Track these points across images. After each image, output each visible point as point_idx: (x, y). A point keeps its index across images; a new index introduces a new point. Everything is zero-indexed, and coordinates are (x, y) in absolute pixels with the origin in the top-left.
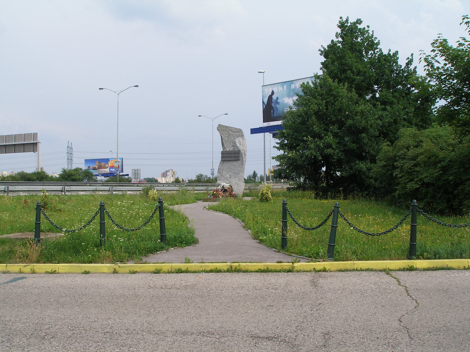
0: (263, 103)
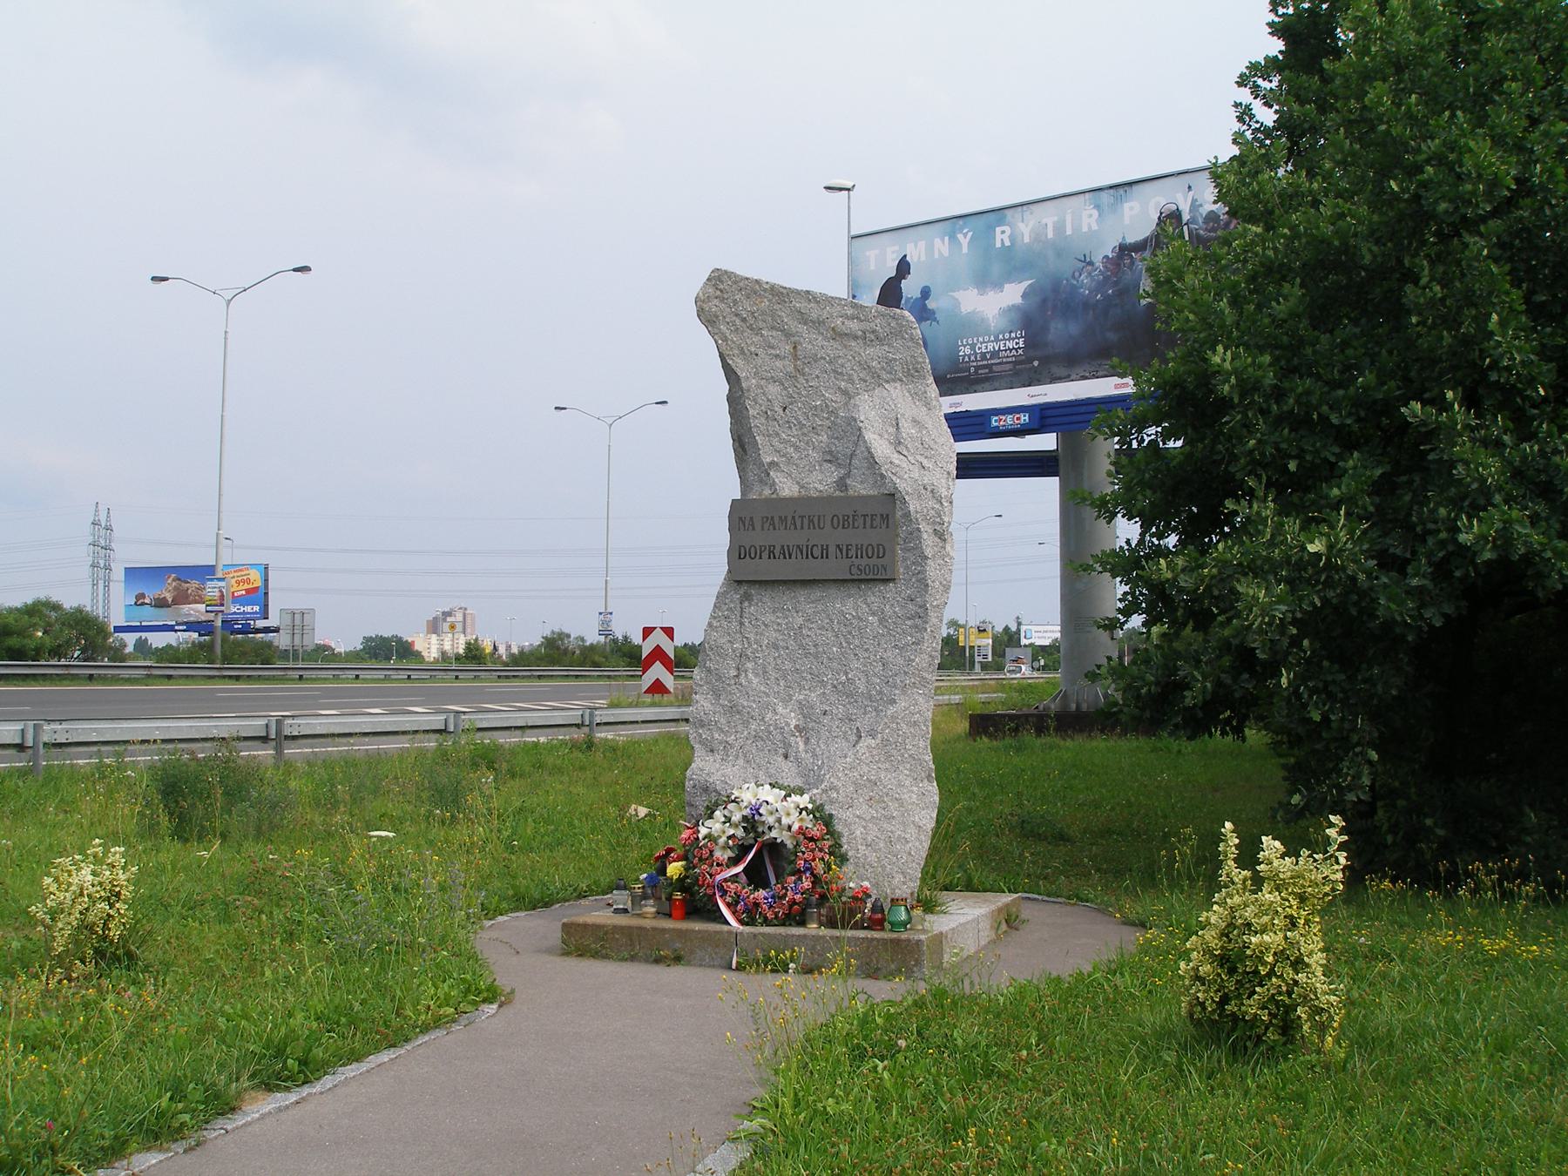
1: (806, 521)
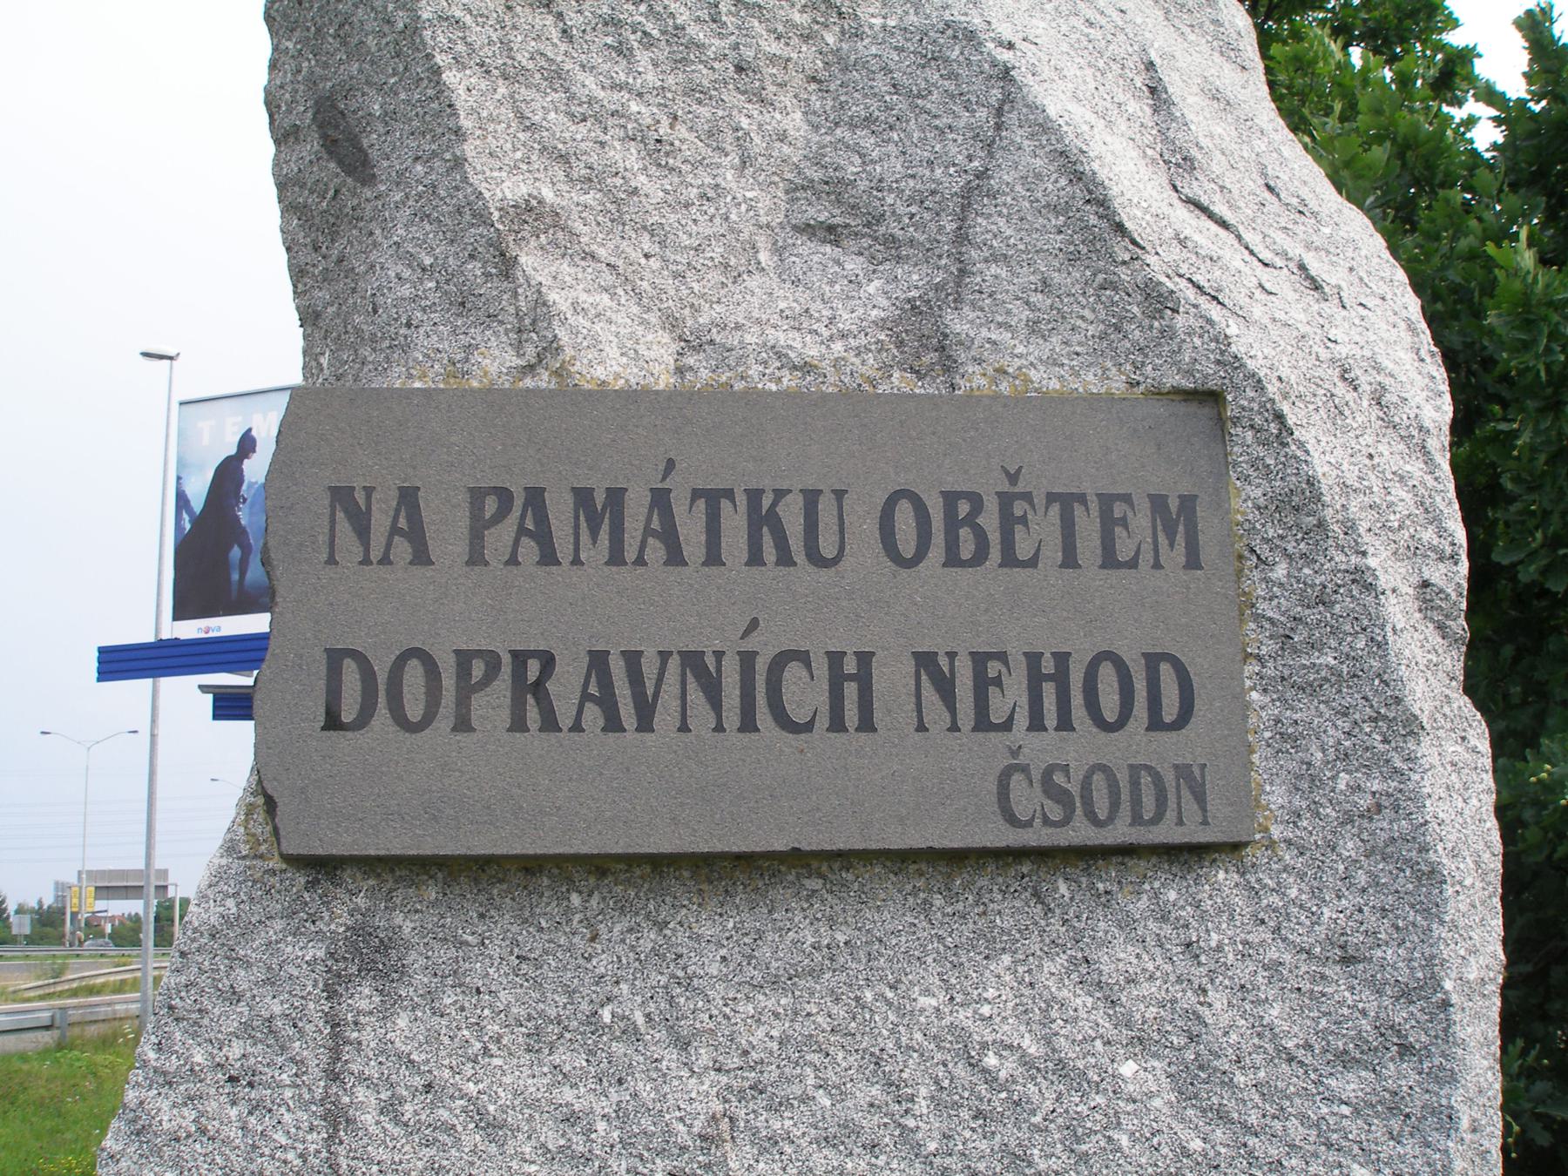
0: (182, 500)
1: (734, 522)
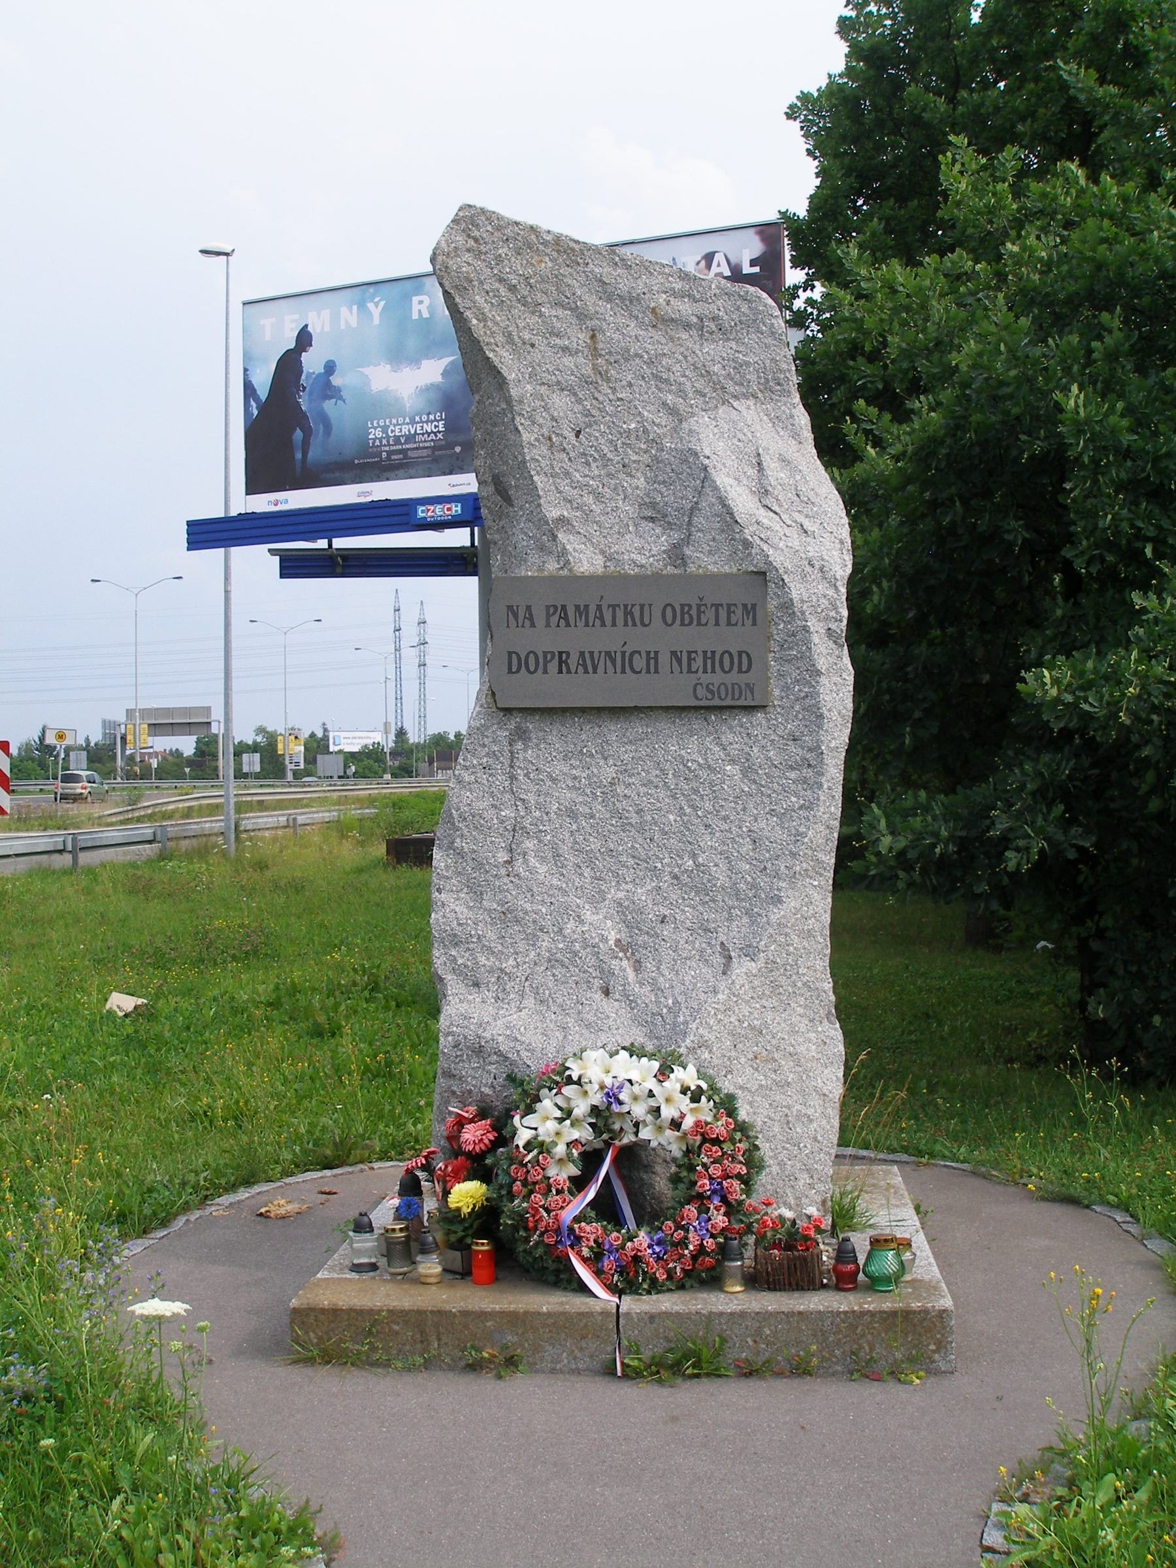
0: (249, 390)
1: (620, 614)
